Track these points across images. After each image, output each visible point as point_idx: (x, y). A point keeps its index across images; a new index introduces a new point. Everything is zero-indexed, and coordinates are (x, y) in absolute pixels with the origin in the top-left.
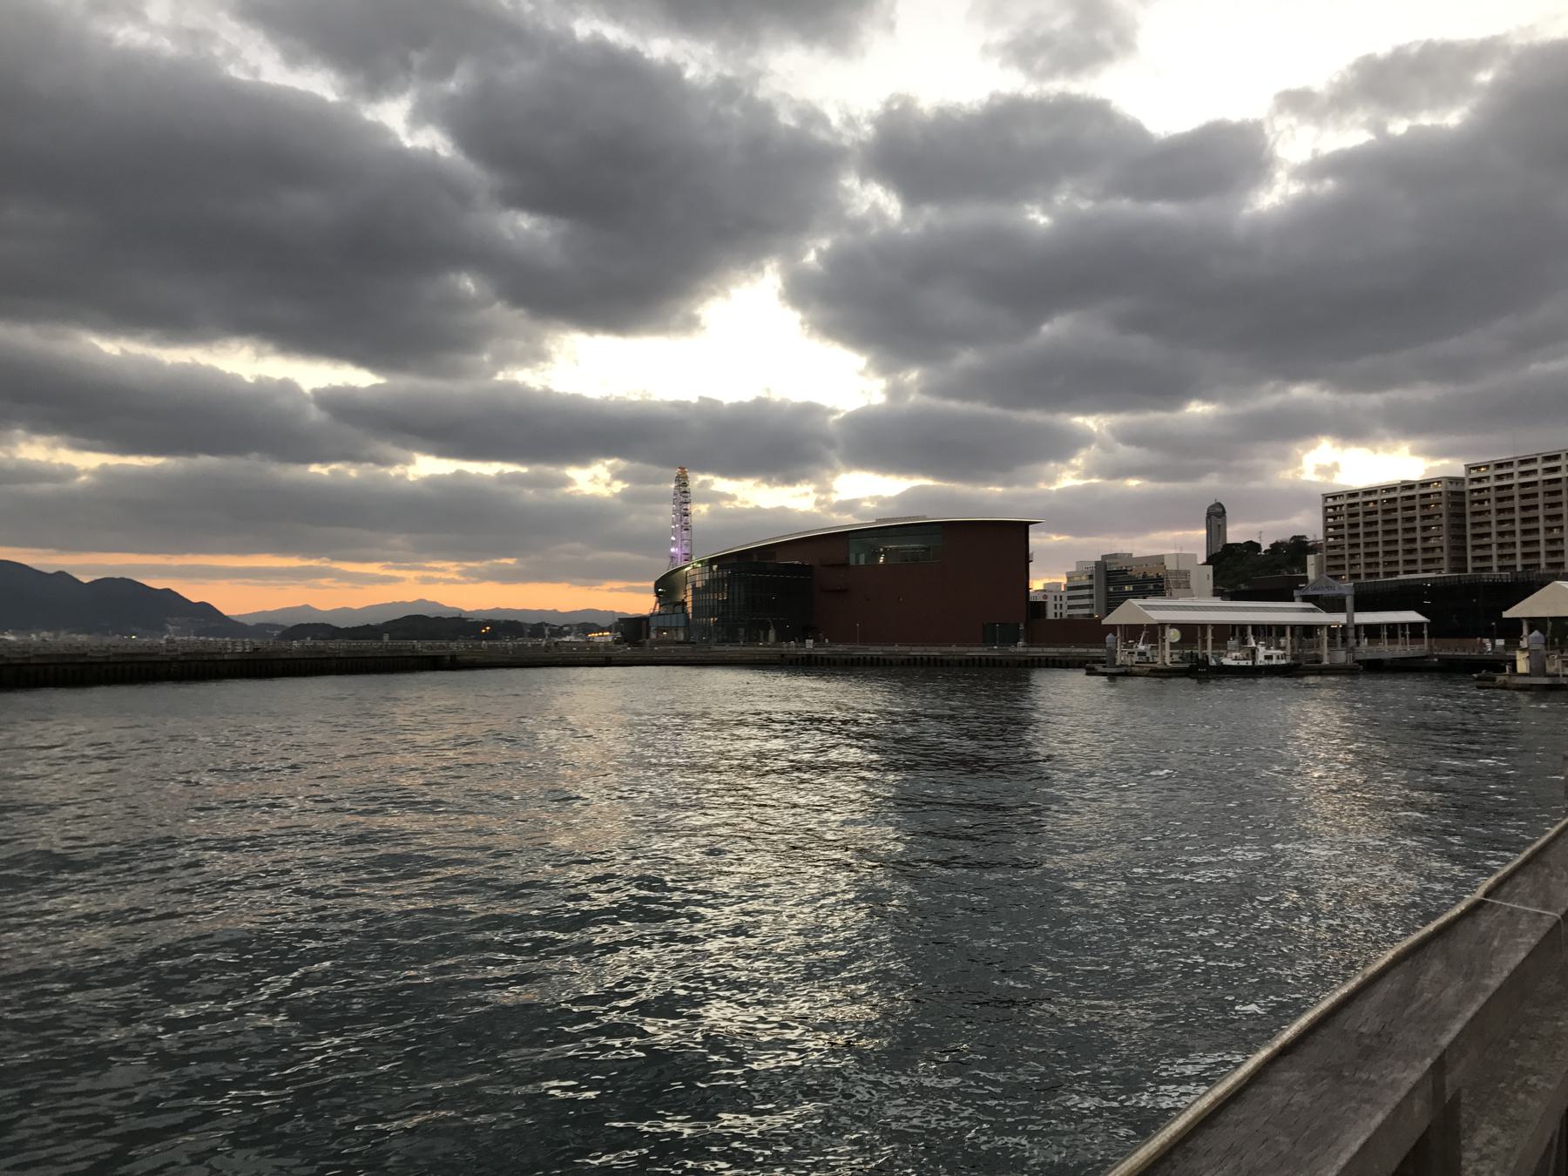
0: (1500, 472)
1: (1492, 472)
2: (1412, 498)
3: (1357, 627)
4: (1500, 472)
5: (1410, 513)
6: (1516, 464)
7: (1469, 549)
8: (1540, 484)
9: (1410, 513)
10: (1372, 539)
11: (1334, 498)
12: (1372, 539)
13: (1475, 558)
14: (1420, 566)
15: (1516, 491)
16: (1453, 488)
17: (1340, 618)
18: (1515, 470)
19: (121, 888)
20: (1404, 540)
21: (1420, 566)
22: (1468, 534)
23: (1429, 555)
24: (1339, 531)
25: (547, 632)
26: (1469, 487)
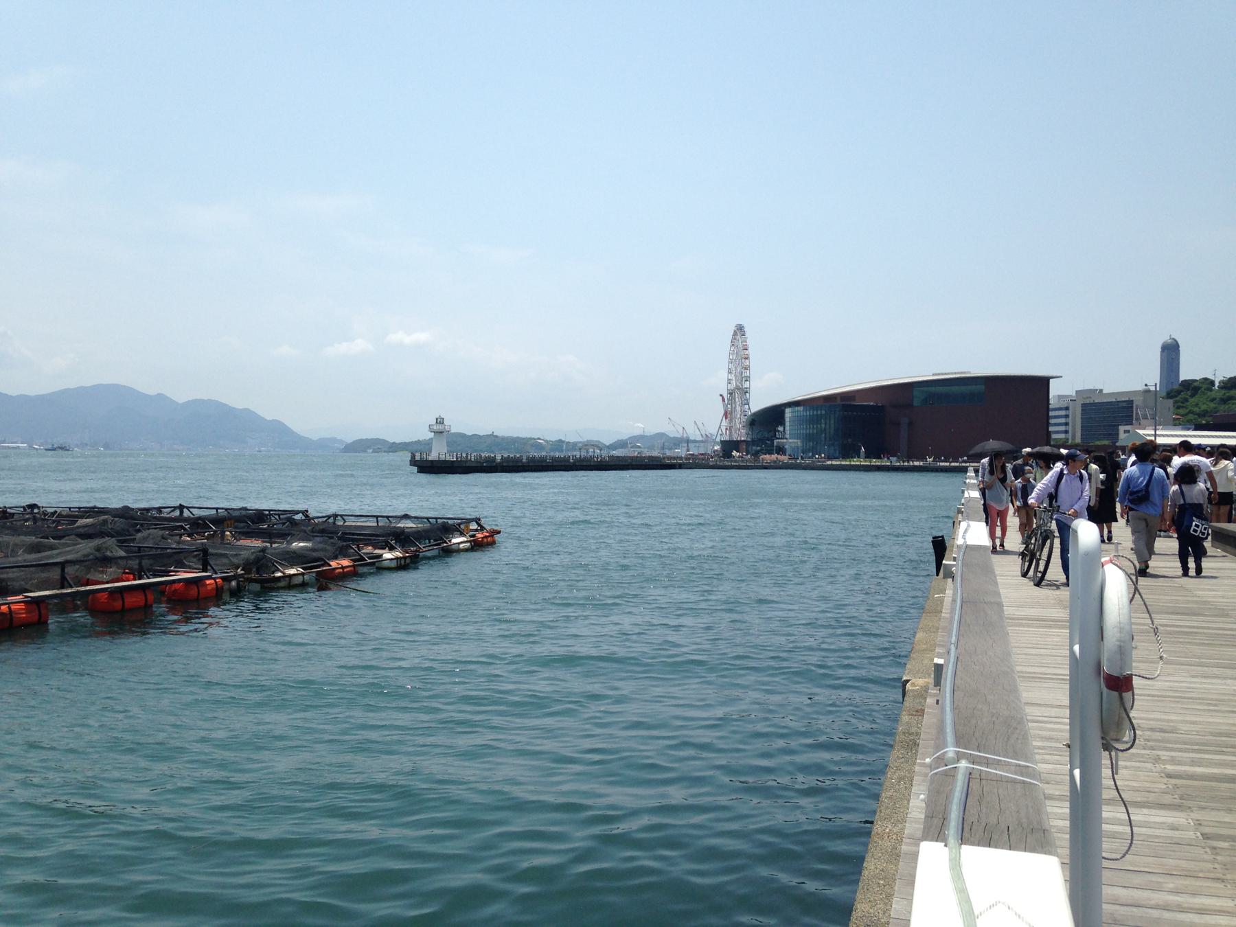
25: (564, 448)
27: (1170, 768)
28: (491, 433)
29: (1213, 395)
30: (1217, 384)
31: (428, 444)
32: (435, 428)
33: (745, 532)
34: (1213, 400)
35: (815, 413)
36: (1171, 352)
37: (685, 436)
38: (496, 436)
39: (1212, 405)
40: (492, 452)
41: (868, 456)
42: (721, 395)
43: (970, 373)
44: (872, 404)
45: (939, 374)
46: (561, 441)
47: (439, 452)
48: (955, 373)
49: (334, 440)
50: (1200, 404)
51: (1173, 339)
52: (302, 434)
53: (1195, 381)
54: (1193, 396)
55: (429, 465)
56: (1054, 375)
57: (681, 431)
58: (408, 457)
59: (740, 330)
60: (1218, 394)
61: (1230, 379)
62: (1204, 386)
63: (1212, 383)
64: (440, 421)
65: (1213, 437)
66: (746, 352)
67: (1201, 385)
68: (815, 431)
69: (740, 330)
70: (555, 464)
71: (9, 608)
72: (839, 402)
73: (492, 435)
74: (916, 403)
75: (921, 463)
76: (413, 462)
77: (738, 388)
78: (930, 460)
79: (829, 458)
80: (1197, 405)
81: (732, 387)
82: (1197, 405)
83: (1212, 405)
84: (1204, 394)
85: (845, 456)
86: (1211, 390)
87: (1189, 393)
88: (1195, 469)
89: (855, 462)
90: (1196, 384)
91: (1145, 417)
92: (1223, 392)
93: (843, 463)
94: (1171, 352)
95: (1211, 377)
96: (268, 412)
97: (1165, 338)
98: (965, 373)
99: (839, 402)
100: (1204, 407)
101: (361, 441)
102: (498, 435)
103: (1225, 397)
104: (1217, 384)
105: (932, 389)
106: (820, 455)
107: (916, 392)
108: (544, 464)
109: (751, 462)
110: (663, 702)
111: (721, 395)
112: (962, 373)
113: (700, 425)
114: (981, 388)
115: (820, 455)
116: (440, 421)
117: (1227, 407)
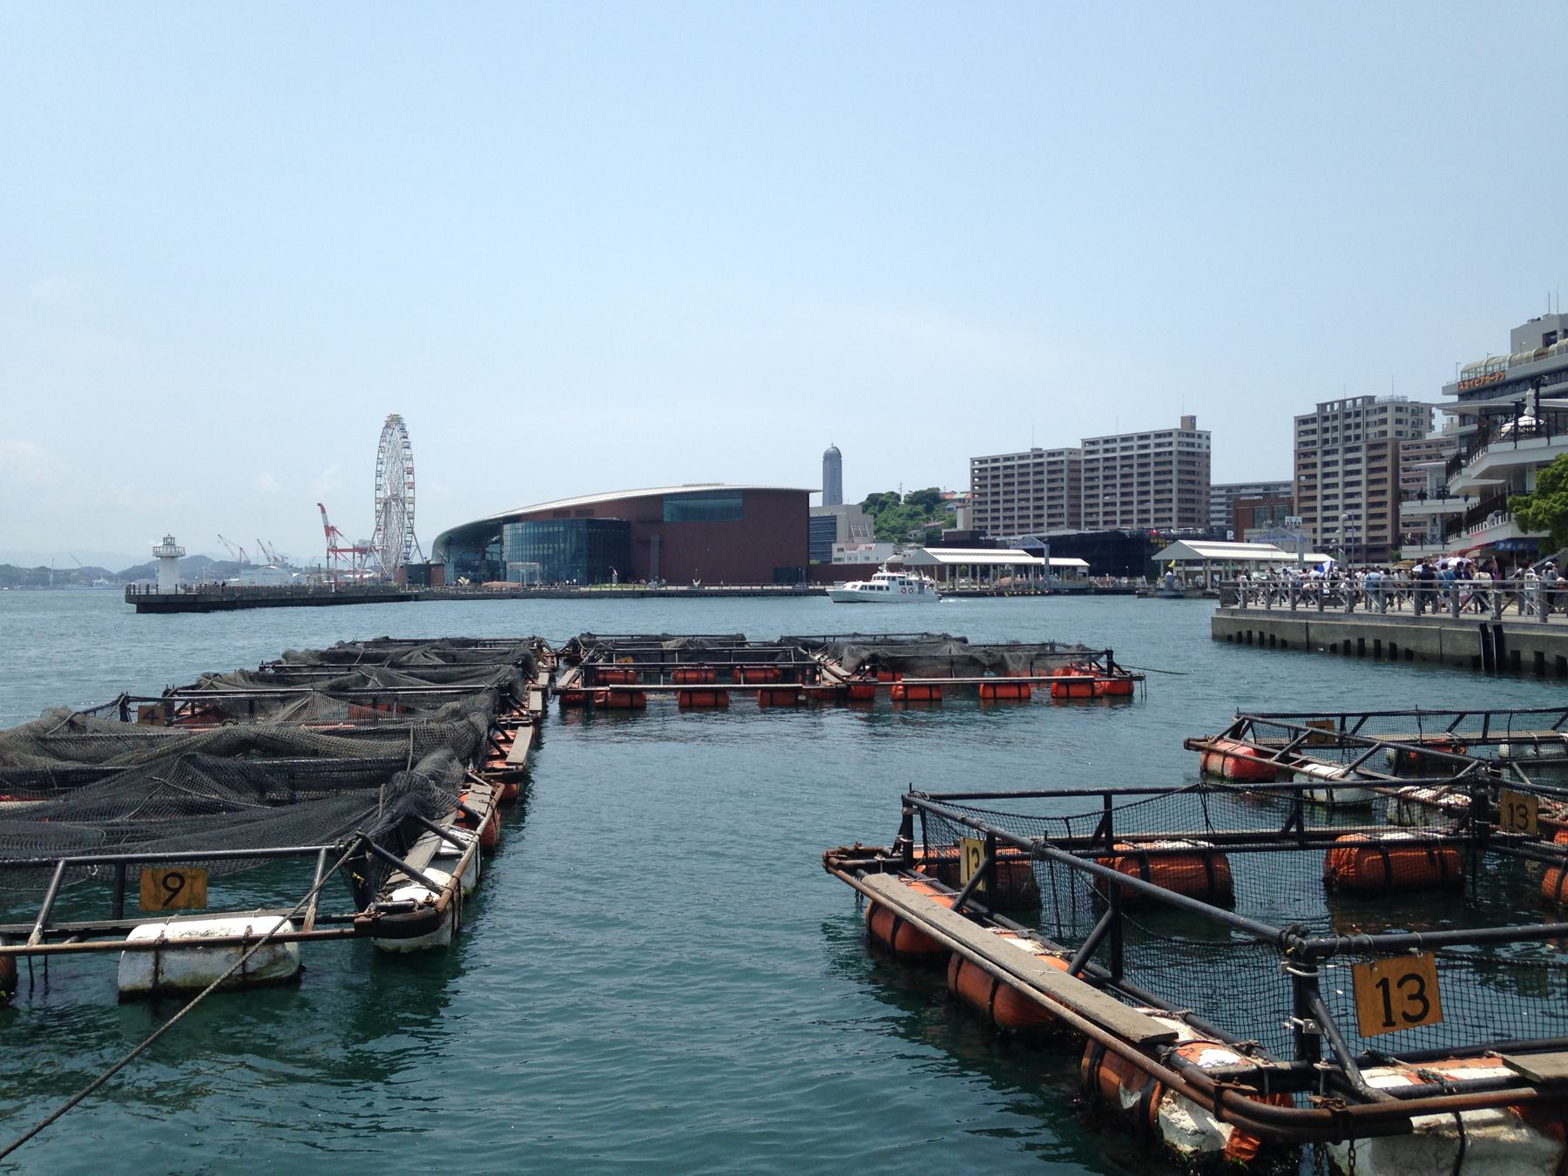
0: (1107, 446)
1: (1135, 443)
2: (1041, 464)
3: (1051, 566)
4: (1107, 446)
5: (1039, 477)
6: (1118, 441)
7: (1083, 498)
8: (1101, 460)
9: (1039, 477)
10: (1039, 495)
11: (981, 462)
12: (1039, 495)
13: (1087, 505)
14: (1016, 530)
15: (1118, 463)
16: (1072, 457)
17: (1041, 561)
18: (1117, 445)
19: (1201, 744)
20: (1086, 487)
21: (1016, 530)
22: (1083, 495)
23: (1053, 511)
24: (983, 491)
25: (51, 578)
26: (1083, 457)
27: (350, 1088)
29: (900, 510)
31: (147, 572)
32: (163, 551)
33: (1193, 677)
34: (900, 515)
35: (541, 530)
37: (244, 559)
39: (900, 521)
40: (219, 578)
41: (623, 579)
42: (319, 505)
43: (723, 484)
45: (690, 486)
46: (43, 569)
47: (167, 584)
48: (708, 485)
53: (882, 495)
54: (880, 511)
56: (815, 489)
57: (237, 552)
58: (123, 593)
59: (395, 422)
61: (916, 493)
62: (891, 501)
63: (898, 497)
64: (169, 541)
65: (995, 555)
66: (408, 452)
68: (551, 552)
69: (395, 422)
70: (295, 597)
71: (1386, 860)
72: (573, 516)
75: (790, 588)
76: (130, 599)
77: (395, 498)
78: (696, 584)
79: (581, 583)
80: (885, 521)
81: (387, 493)
82: (885, 521)
83: (900, 521)
85: (591, 581)
86: (898, 505)
87: (877, 508)
89: (606, 588)
90: (883, 498)
91: (858, 535)
92: (910, 506)
93: (593, 589)
94: (833, 461)
95: (897, 491)
97: (827, 447)
99: (573, 516)
100: (893, 523)
101: (89, 568)
103: (911, 513)
104: (903, 499)
105: (685, 503)
106: (571, 580)
108: (284, 597)
109: (470, 591)
110: (587, 1017)
111: (319, 505)
112: (715, 485)
114: (739, 502)
115: (571, 580)
116: (169, 541)
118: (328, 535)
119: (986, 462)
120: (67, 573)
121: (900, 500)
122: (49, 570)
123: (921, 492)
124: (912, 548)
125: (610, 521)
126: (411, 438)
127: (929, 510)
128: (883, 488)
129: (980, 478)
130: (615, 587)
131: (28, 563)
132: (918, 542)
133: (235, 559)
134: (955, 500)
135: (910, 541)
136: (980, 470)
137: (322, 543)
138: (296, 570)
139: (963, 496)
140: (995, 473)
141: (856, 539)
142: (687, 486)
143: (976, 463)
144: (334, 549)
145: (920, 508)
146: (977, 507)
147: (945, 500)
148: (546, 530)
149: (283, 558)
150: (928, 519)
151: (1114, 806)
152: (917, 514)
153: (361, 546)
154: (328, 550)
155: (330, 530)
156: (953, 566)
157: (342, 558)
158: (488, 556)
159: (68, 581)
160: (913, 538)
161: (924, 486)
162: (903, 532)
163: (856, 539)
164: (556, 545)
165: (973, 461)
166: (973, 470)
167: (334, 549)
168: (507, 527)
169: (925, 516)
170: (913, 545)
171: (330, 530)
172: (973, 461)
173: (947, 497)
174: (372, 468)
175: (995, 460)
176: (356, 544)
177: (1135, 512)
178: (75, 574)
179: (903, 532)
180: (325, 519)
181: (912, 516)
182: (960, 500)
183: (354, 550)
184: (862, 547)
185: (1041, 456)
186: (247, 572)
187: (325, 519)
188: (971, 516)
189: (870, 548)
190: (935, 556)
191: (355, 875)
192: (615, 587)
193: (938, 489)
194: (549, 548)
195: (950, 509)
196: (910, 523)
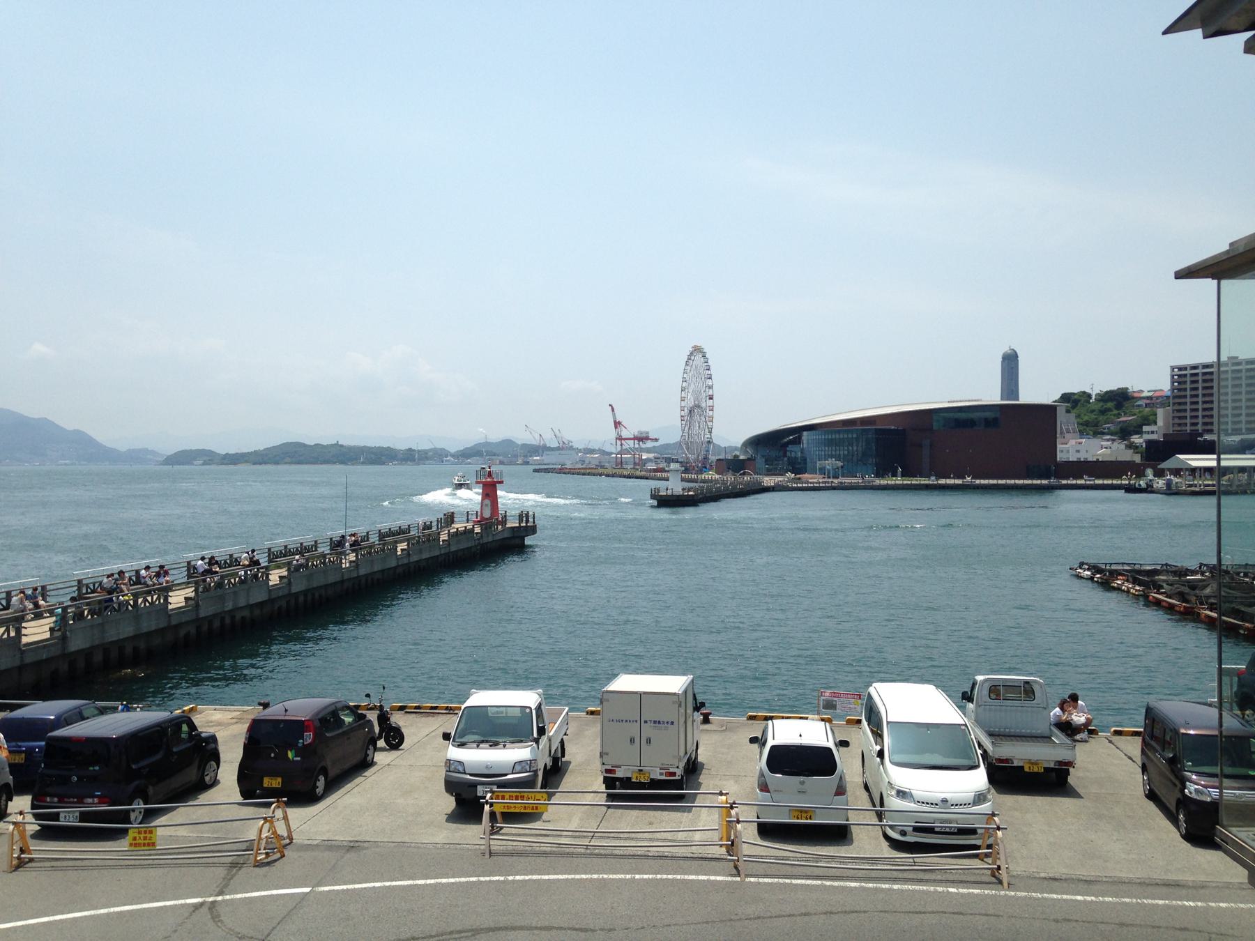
11: (1180, 369)
28: (336, 442)
30: (1094, 397)
34: (1093, 411)
35: (823, 437)
36: (1010, 362)
37: (542, 443)
38: (342, 446)
42: (610, 405)
43: (981, 400)
44: (893, 427)
46: (410, 449)
49: (153, 452)
50: (1082, 415)
51: (1013, 350)
52: (109, 445)
53: (1074, 394)
55: (674, 499)
57: (538, 437)
60: (1096, 406)
61: (1107, 392)
62: (1083, 399)
63: (1089, 396)
67: (1080, 398)
73: (337, 444)
74: (935, 426)
78: (969, 479)
81: (690, 402)
83: (1093, 416)
84: (1083, 406)
88: (872, 460)
89: (891, 481)
90: (1076, 397)
91: (1068, 432)
92: (1101, 404)
94: (1010, 362)
95: (1088, 391)
96: (69, 424)
97: (1006, 349)
98: (978, 400)
100: (1086, 418)
102: (344, 444)
104: (1094, 397)
107: (935, 417)
111: (610, 405)
113: (557, 432)
117: (1106, 417)
118: (616, 427)
119: (1185, 369)
120: (426, 452)
121: (1091, 398)
122: (414, 450)
123: (1111, 392)
124: (1108, 440)
125: (890, 430)
126: (710, 363)
127: (1119, 406)
128: (1075, 389)
129: (1179, 383)
130: (899, 481)
131: (401, 446)
132: (1112, 435)
133: (536, 443)
134: (1144, 398)
135: (1104, 434)
136: (1179, 376)
137: (612, 434)
138: (580, 451)
139: (1150, 394)
140: (1194, 378)
141: (1067, 435)
142: (951, 402)
143: (1176, 370)
144: (620, 438)
145: (1110, 405)
146: (1177, 407)
147: (1133, 398)
148: (830, 437)
149: (569, 442)
150: (1119, 414)
151: (292, 830)
152: (1109, 410)
153: (639, 436)
154: (616, 439)
155: (617, 424)
156: (1200, 468)
157: (625, 444)
158: (788, 454)
159: (427, 458)
160: (1106, 431)
161: (1113, 386)
162: (1096, 425)
163: (1067, 435)
164: (850, 448)
165: (1173, 368)
166: (1172, 376)
167: (620, 438)
168: (805, 433)
169: (1115, 412)
170: (1108, 437)
171: (617, 424)
172: (1173, 368)
173: (1136, 395)
174: (678, 383)
175: (1195, 367)
176: (636, 434)
177: (1244, 378)
178: (431, 453)
179: (1096, 425)
180: (614, 415)
181: (1103, 412)
182: (1148, 398)
183: (634, 439)
184: (1072, 442)
185: (1239, 364)
186: (548, 453)
187: (614, 415)
188: (1171, 415)
189: (1080, 443)
190: (1187, 461)
191: (91, 768)
192: (899, 481)
193: (1127, 388)
194: (836, 450)
195: (1139, 406)
196: (1101, 418)
